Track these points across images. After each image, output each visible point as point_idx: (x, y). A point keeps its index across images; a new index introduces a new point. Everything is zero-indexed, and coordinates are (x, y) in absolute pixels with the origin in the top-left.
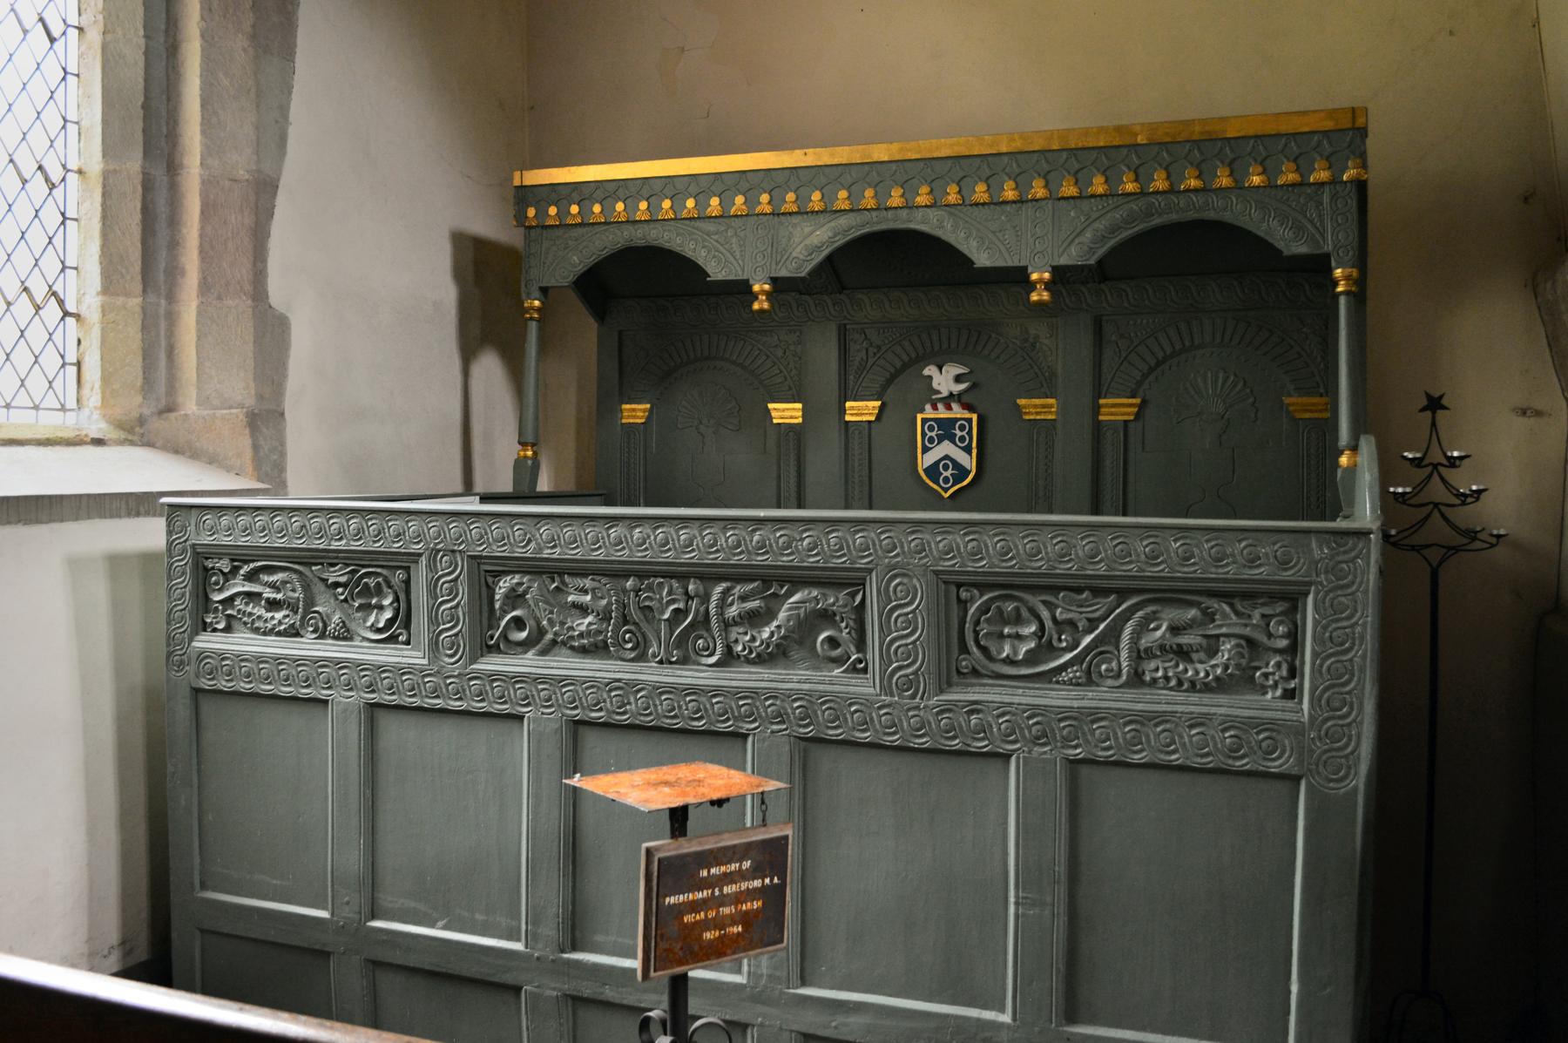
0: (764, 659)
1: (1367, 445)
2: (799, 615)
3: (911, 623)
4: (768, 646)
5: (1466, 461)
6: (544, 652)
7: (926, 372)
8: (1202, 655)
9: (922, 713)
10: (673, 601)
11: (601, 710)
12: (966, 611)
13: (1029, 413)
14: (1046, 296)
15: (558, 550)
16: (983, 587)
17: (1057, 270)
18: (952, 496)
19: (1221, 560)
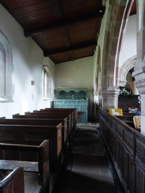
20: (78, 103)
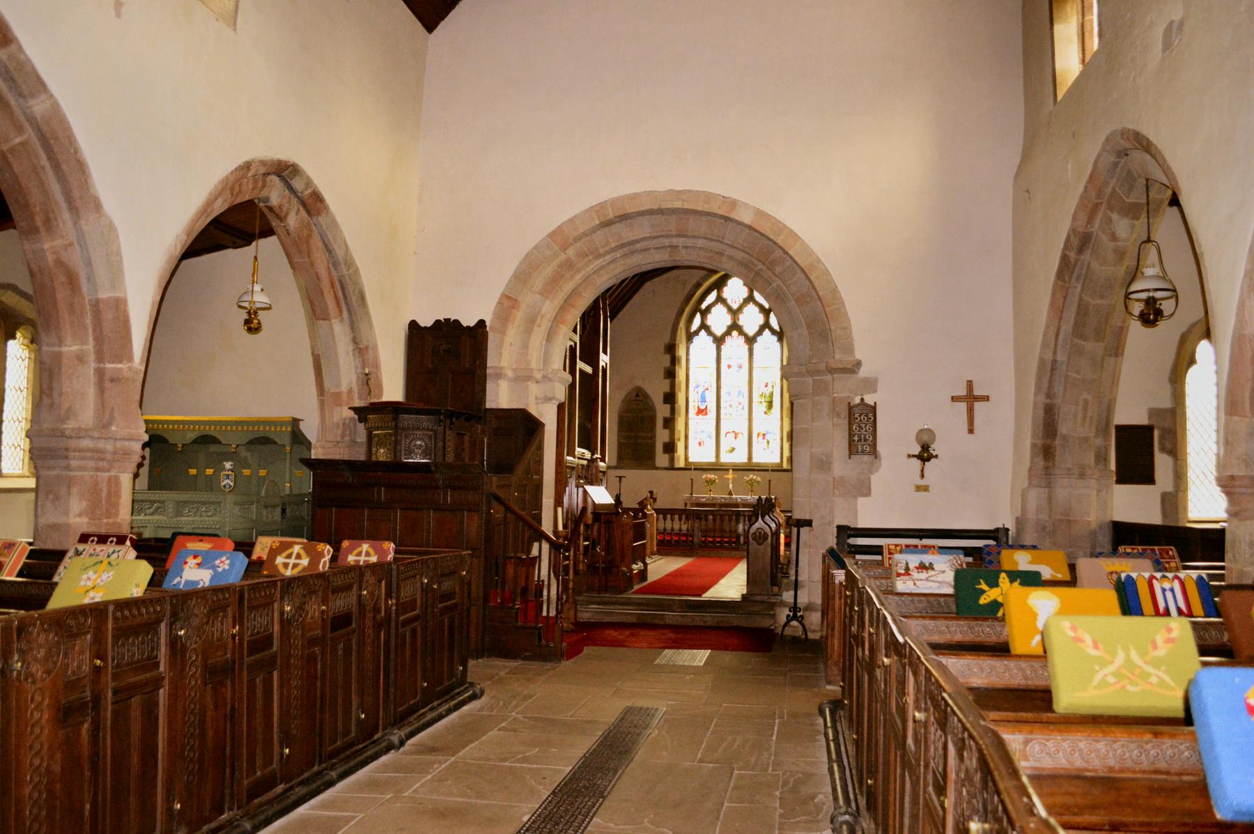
17: (183, 445)
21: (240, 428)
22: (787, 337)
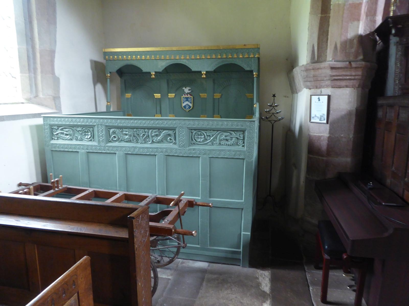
0: (158, 142)
1: (258, 104)
2: (164, 135)
3: (102, 136)
4: (159, 140)
5: (278, 106)
6: (120, 142)
7: (183, 89)
8: (230, 140)
9: (185, 151)
10: (143, 133)
11: (130, 152)
12: (192, 134)
13: (202, 96)
14: (205, 76)
15: (121, 124)
16: (195, 130)
17: (207, 72)
18: (188, 111)
19: (232, 125)
20: (192, 141)
21: (153, 57)
22: (374, 26)
